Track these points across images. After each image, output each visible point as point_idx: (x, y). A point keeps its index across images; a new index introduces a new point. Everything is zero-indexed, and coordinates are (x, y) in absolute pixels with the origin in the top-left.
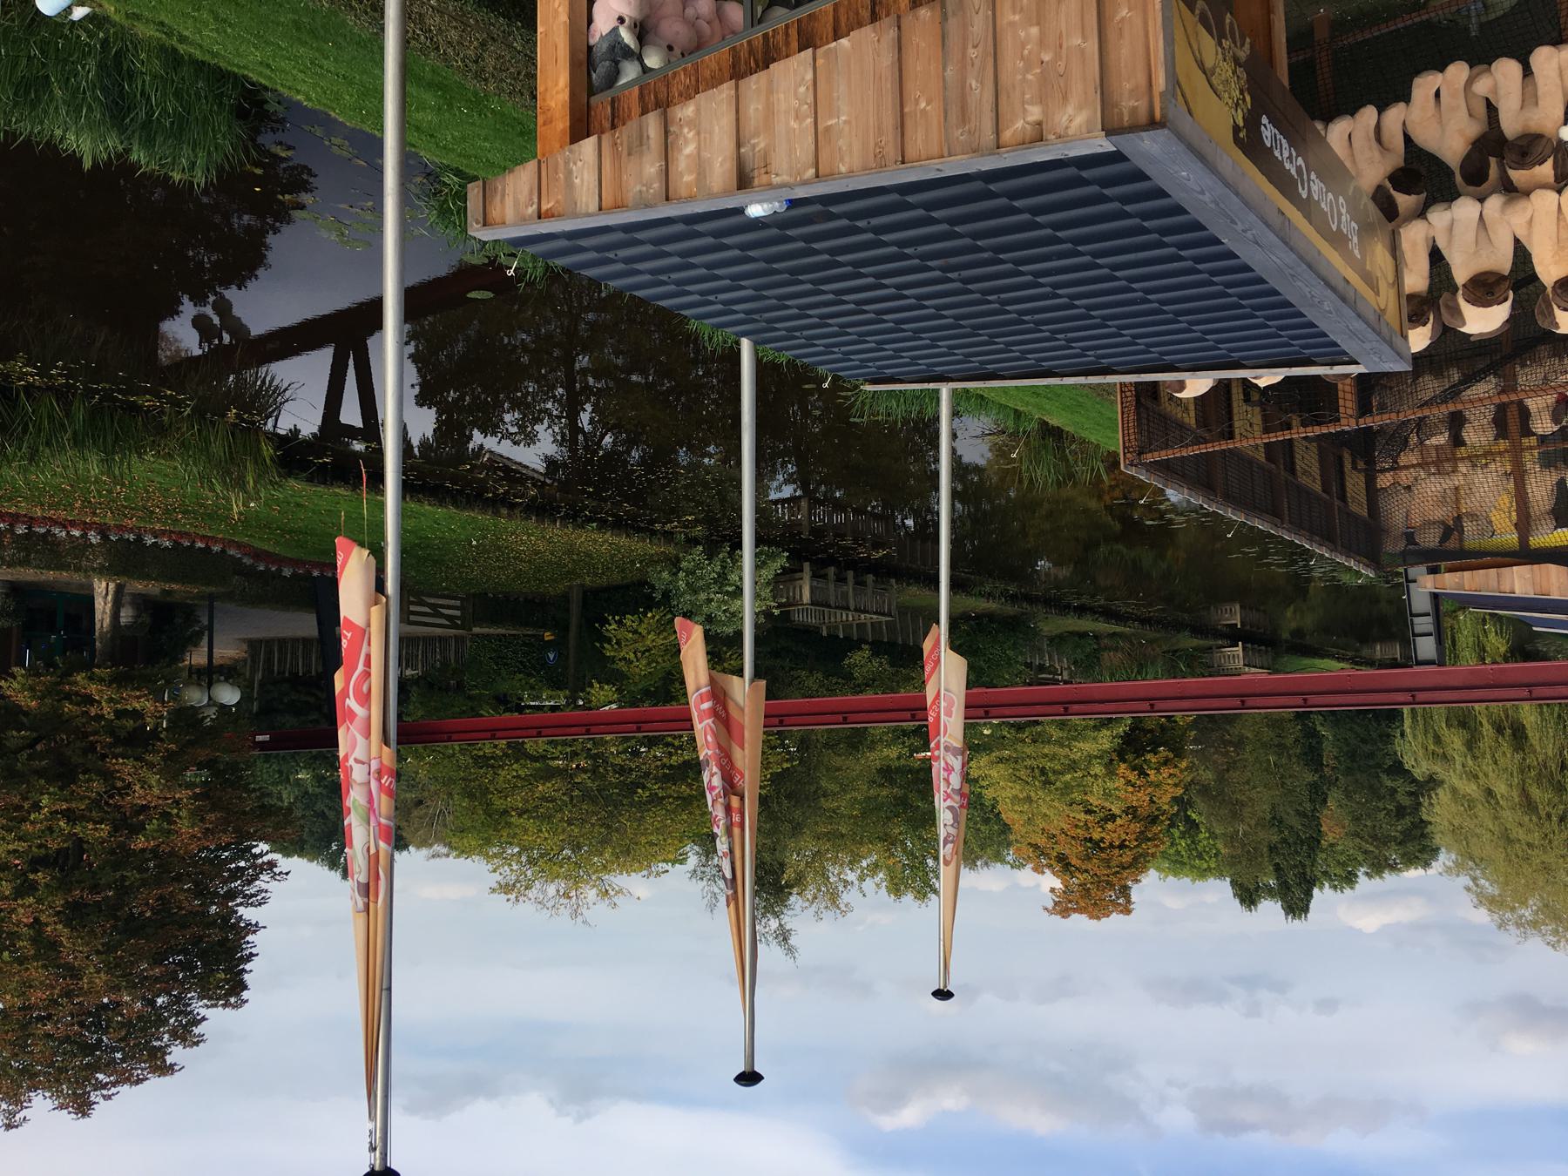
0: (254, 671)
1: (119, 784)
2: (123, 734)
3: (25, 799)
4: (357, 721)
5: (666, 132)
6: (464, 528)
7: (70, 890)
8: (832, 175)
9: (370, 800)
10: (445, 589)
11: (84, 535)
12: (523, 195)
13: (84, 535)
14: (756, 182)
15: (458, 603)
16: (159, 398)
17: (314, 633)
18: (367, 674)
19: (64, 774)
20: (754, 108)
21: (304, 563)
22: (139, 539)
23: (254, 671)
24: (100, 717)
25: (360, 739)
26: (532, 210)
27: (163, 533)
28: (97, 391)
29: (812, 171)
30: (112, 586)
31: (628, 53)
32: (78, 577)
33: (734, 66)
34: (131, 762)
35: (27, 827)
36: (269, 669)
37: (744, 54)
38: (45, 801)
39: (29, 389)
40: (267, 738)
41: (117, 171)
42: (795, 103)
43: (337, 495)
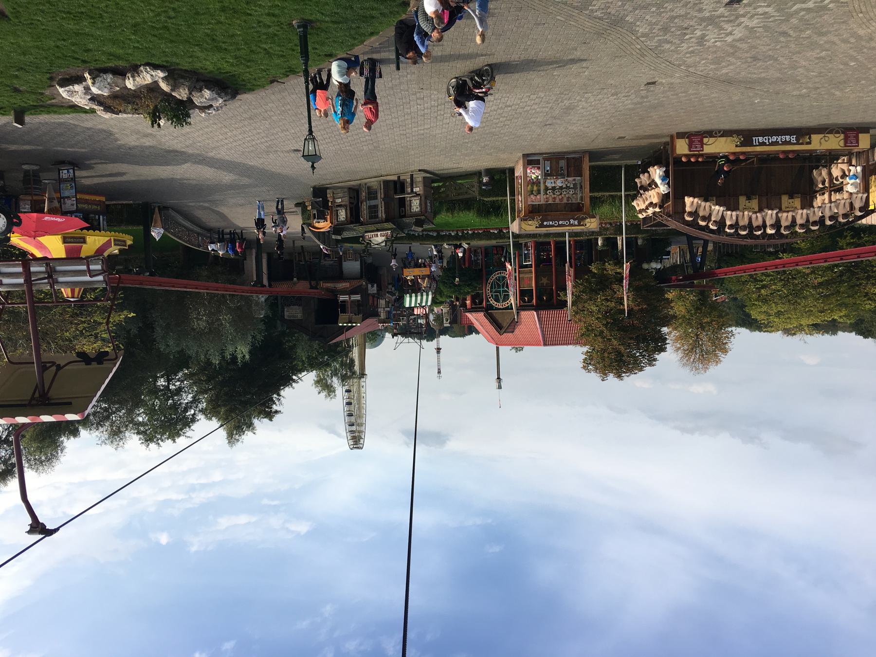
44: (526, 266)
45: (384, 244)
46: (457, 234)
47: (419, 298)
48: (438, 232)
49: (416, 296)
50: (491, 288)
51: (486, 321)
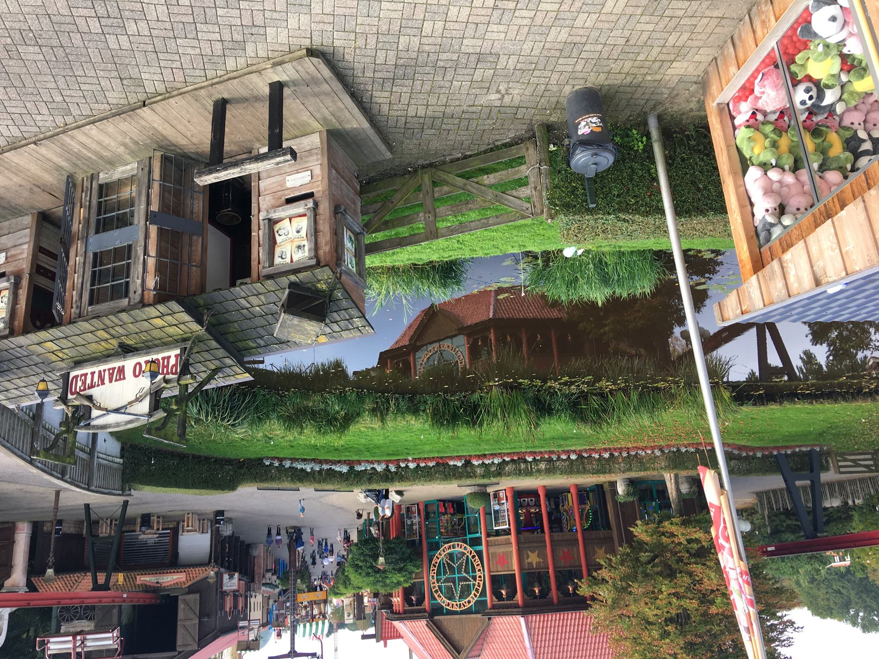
0: (763, 510)
1: (697, 578)
2: (693, 552)
3: (655, 588)
4: (726, 550)
5: (782, 268)
6: (855, 413)
7: (685, 636)
8: (853, 273)
9: (741, 587)
10: (858, 449)
11: (653, 452)
12: (734, 306)
13: (653, 452)
14: (823, 282)
15: (869, 456)
16: (667, 382)
17: (783, 485)
18: (725, 528)
19: (671, 574)
20: (814, 249)
21: (767, 448)
22: (679, 450)
23: (763, 510)
24: (680, 544)
25: (730, 558)
26: (739, 311)
27: (689, 444)
28: (639, 386)
29: (844, 273)
30: (672, 475)
31: (772, 225)
32: (655, 473)
33: (815, 221)
34: (699, 566)
35: (658, 602)
36: (771, 508)
37: (818, 215)
38: (664, 588)
39: (611, 391)
40: (773, 548)
41: (614, 303)
42: (829, 244)
43: (772, 409)
44: (498, 533)
45: (144, 407)
46: (387, 469)
47: (314, 626)
48: (351, 464)
49: (311, 626)
50: (438, 573)
51: (431, 635)
